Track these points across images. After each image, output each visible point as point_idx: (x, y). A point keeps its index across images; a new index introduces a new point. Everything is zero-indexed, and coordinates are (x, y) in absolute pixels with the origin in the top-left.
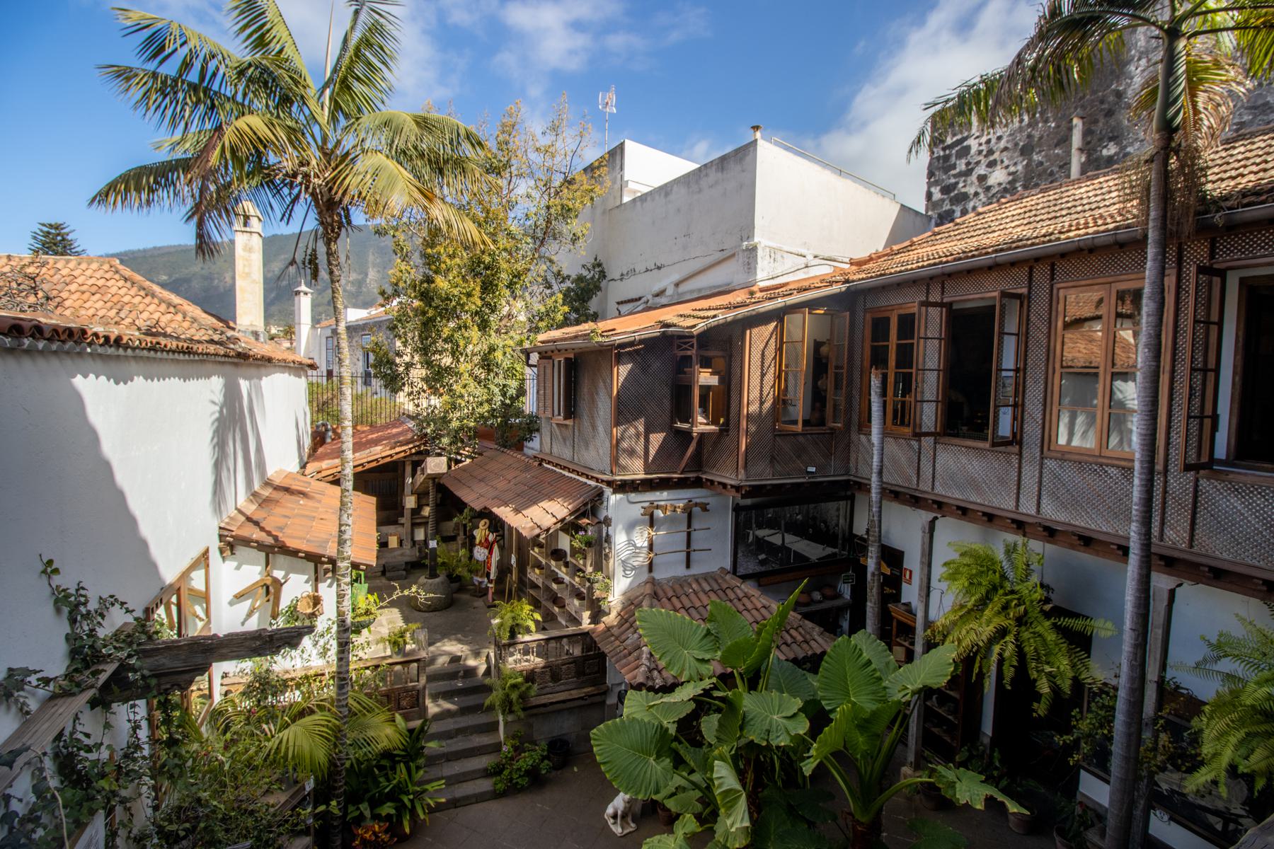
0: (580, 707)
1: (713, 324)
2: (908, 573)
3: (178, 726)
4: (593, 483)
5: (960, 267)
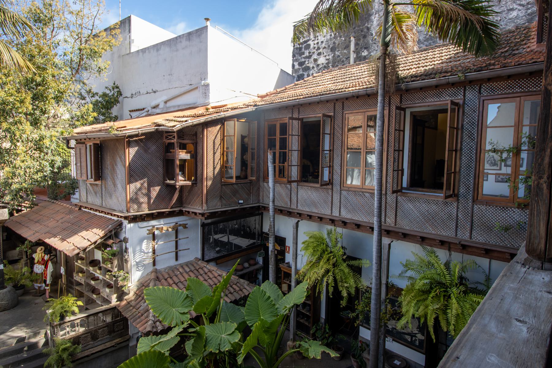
1: (185, 125)
4: (115, 218)
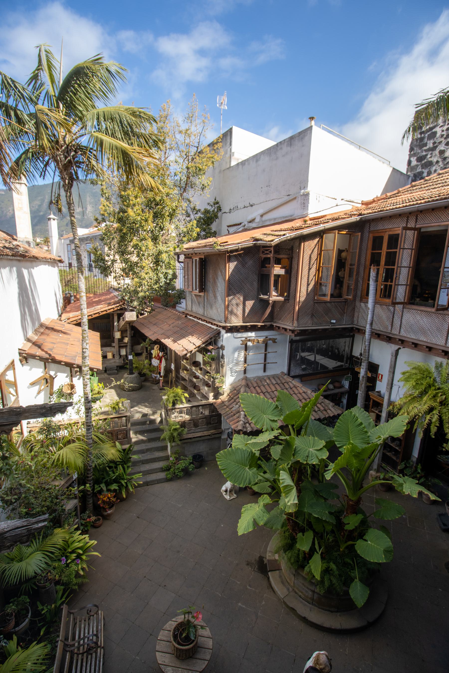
0: (209, 439)
1: (283, 240)
2: (380, 376)
3: (7, 451)
4: (215, 327)
5: (428, 207)
